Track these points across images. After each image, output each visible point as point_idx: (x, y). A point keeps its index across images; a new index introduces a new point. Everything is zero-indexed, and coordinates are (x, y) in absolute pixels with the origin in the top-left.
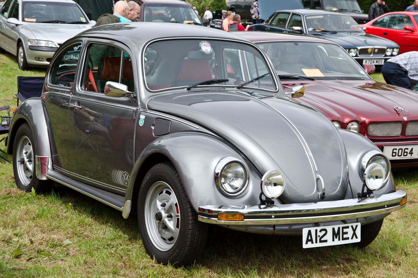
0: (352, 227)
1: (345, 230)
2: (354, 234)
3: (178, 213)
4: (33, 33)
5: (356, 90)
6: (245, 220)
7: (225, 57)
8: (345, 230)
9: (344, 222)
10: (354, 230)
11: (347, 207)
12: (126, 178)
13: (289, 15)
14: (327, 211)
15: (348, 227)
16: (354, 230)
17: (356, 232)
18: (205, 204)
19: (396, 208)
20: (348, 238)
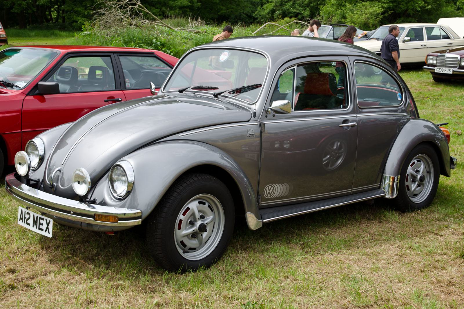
0: (46, 220)
1: (41, 221)
2: (47, 228)
3: (181, 221)
4: (446, 34)
5: (131, 109)
6: (119, 221)
7: (383, 31)
8: (41, 221)
9: (43, 214)
10: (48, 225)
11: (113, 214)
12: (269, 190)
13: (114, 89)
14: (55, 206)
15: (43, 219)
16: (48, 225)
17: (46, 226)
18: (98, 202)
19: (19, 199)
20: (42, 230)
